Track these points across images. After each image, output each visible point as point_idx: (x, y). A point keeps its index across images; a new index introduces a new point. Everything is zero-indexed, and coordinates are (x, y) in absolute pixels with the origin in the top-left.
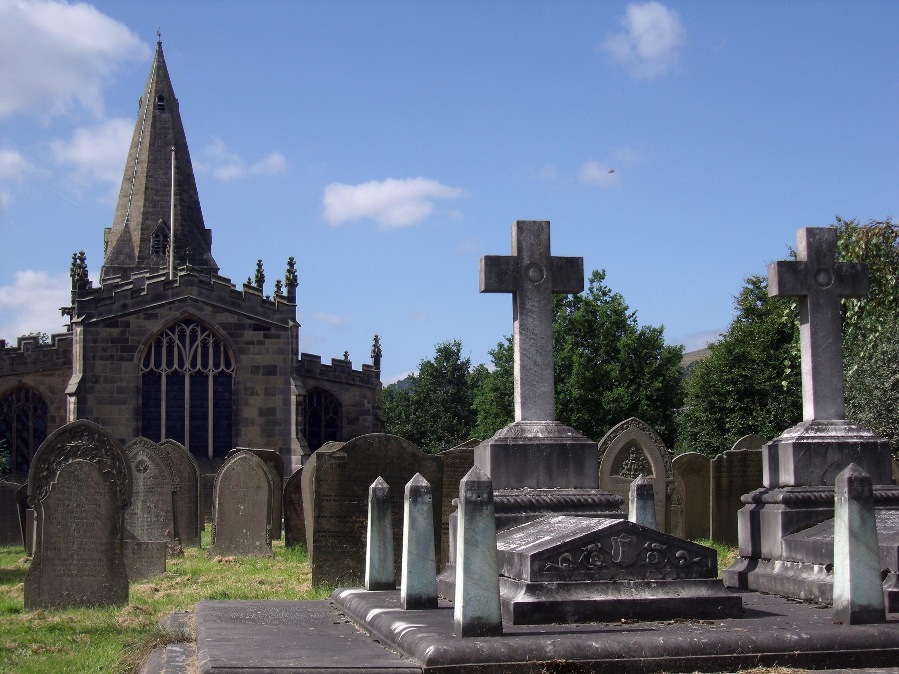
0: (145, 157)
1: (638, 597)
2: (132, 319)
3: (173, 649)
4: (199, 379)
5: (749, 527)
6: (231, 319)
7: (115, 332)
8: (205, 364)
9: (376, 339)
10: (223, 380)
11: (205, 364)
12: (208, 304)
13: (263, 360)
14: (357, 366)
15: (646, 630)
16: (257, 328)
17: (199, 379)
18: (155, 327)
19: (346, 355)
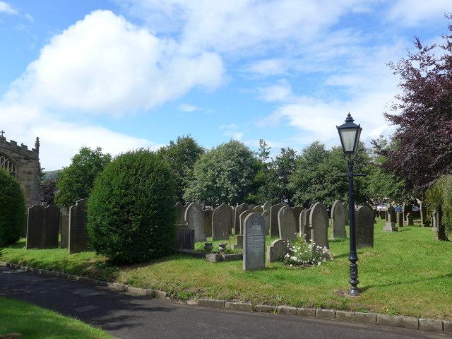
6: (17, 155)
9: (38, 139)
14: (30, 149)
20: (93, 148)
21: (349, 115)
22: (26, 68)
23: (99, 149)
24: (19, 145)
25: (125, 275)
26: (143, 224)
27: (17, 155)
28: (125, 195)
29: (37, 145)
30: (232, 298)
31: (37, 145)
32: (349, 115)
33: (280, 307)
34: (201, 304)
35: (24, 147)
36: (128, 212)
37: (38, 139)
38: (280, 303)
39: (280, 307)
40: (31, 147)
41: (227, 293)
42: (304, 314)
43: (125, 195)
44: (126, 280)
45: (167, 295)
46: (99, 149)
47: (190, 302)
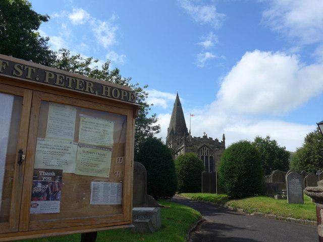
0: (175, 114)
1: (312, 187)
2: (194, 146)
3: (182, 207)
4: (207, 157)
5: (12, 105)
6: (213, 146)
7: (191, 148)
8: (208, 154)
9: (224, 135)
10: (211, 157)
11: (208, 154)
12: (130, 102)
13: (219, 154)
14: (220, 141)
15: (111, 112)
16: (218, 148)
17: (207, 157)
18: (199, 147)
19: (205, 133)
20: (264, 137)
21: (45, 19)
22: (217, 88)
23: (268, 137)
24: (214, 139)
25: (232, 202)
26: (240, 178)
27: (213, 146)
28: (231, 164)
29: (224, 139)
30: (269, 213)
31: (224, 139)
32: (45, 19)
33: (288, 218)
34: (255, 215)
35: (217, 140)
36: (233, 172)
37: (224, 135)
38: (290, 216)
39: (288, 218)
40: (220, 140)
41: (268, 210)
42: (299, 222)
43: (231, 164)
44: (231, 204)
45: (244, 211)
46: (268, 137)
47: (251, 214)
